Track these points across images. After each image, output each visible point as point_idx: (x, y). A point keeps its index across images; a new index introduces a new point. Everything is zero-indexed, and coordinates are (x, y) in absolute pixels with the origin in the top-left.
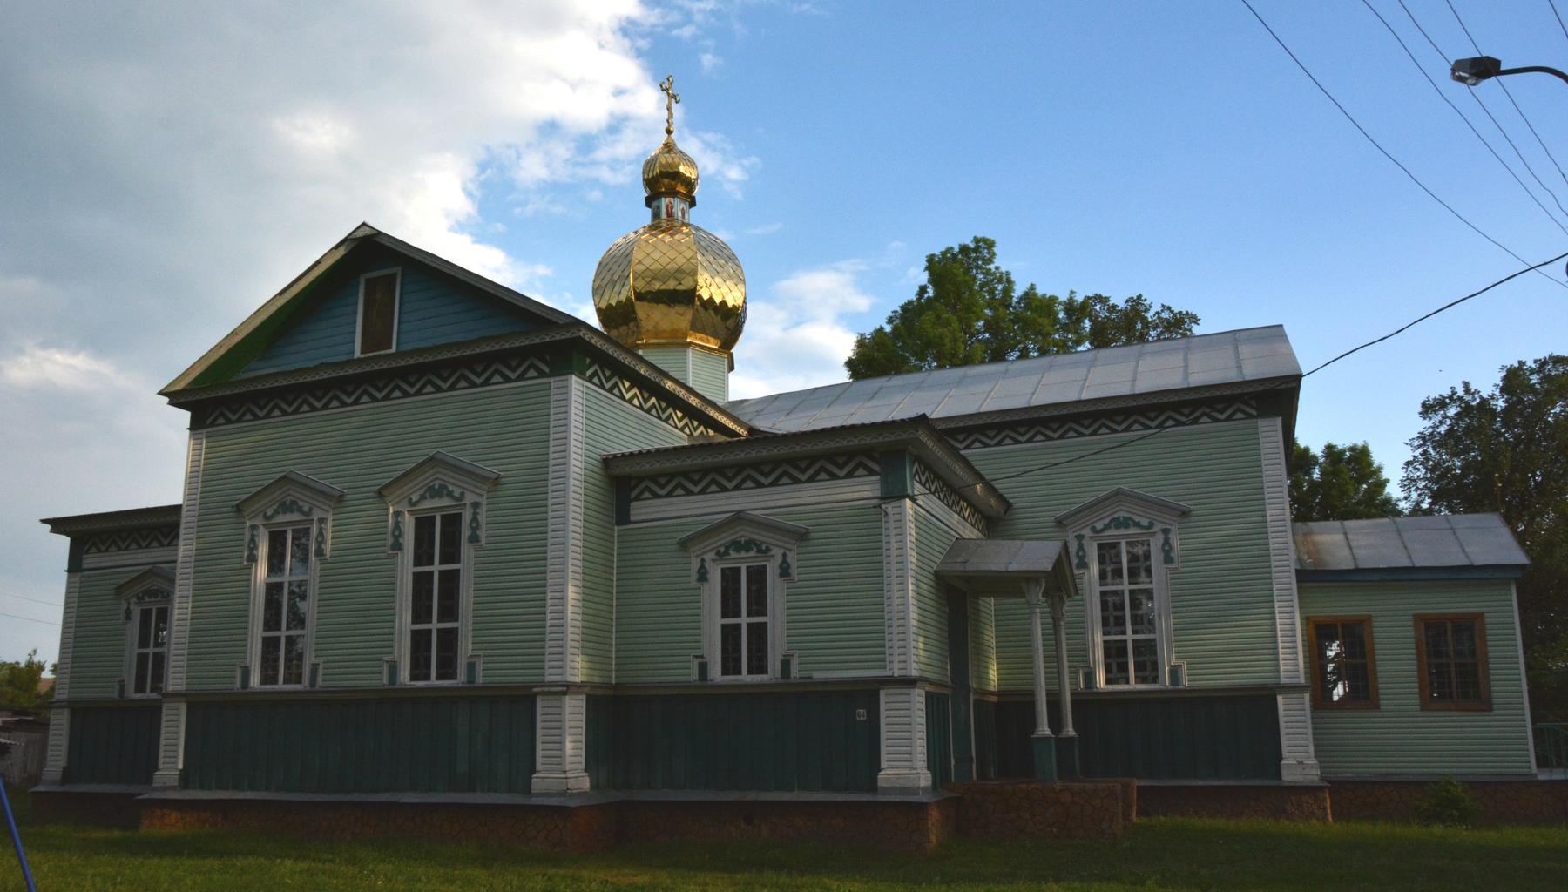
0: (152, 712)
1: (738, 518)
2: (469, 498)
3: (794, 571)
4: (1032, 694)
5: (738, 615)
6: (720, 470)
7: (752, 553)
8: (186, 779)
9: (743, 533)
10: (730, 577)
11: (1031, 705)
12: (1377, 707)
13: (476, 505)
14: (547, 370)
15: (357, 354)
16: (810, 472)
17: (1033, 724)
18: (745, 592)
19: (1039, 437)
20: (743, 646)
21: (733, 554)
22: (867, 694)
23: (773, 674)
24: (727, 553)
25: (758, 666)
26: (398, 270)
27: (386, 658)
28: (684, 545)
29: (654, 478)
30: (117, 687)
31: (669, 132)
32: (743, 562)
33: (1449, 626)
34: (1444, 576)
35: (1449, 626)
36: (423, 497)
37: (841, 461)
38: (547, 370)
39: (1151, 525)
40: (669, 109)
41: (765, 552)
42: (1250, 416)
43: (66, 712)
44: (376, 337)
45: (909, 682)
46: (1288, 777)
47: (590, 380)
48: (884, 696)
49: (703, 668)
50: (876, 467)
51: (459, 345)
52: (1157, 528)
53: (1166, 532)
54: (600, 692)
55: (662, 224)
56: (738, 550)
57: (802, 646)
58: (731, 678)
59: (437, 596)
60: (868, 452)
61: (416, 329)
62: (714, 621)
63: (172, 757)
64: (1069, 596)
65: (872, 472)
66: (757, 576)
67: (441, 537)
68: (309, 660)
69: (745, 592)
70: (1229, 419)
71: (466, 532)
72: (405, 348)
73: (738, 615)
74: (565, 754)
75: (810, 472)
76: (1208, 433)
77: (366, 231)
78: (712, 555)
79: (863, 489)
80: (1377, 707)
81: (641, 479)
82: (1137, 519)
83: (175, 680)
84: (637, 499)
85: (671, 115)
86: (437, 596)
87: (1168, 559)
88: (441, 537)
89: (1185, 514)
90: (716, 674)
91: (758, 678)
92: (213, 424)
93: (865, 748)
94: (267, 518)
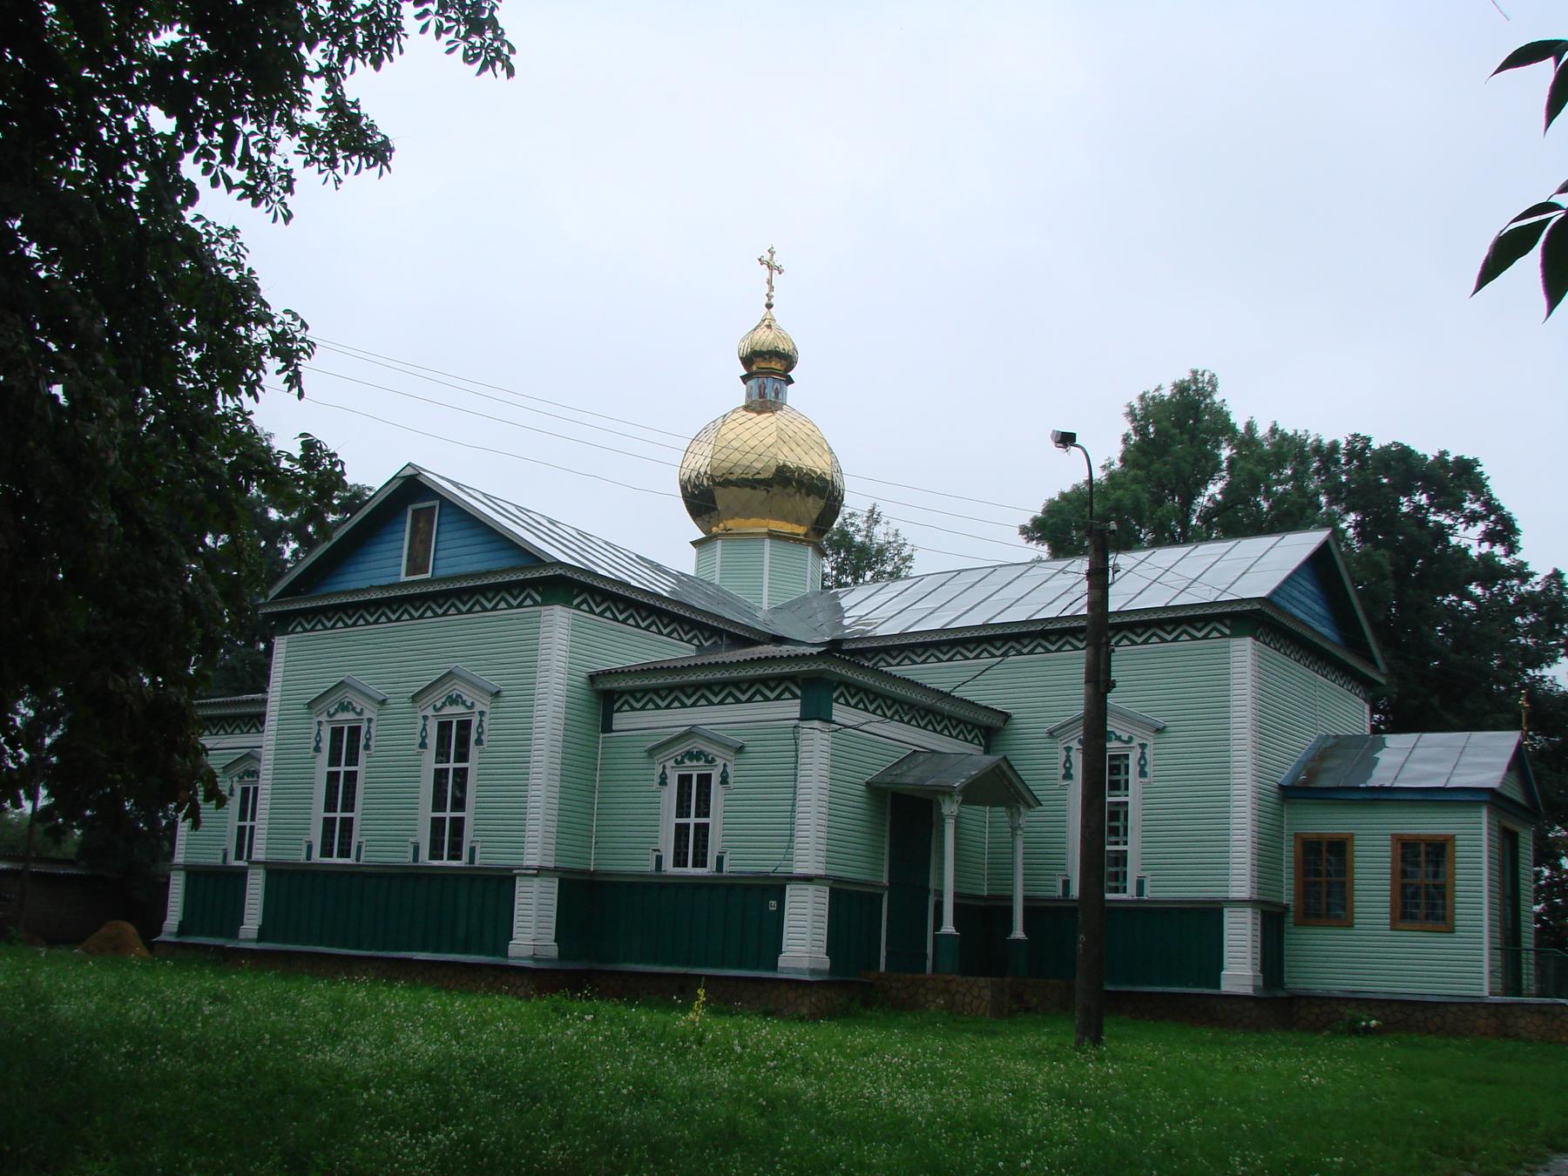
0: (240, 876)
1: (691, 732)
2: (478, 707)
3: (731, 780)
4: (1010, 898)
5: (688, 816)
6: (682, 688)
7: (702, 763)
8: (262, 935)
9: (698, 745)
10: (684, 781)
11: (1009, 911)
12: (1351, 925)
13: (482, 713)
14: (539, 599)
15: (403, 578)
16: (721, 697)
17: (1009, 928)
18: (694, 795)
19: (1068, 647)
20: (693, 842)
21: (687, 763)
22: (773, 888)
23: (709, 870)
24: (682, 762)
25: (700, 861)
26: (437, 503)
27: (412, 839)
28: (652, 752)
29: (632, 692)
30: (411, 850)
31: (769, 306)
32: (695, 769)
33: (1423, 848)
34: (1468, 797)
35: (1423, 848)
36: (444, 704)
37: (772, 684)
38: (539, 599)
39: (1130, 739)
40: (770, 282)
41: (711, 762)
42: (1224, 635)
43: (183, 873)
44: (416, 565)
45: (807, 879)
46: (1227, 986)
47: (578, 607)
48: (790, 890)
49: (659, 860)
50: (799, 693)
51: (488, 573)
52: (1135, 743)
53: (1143, 746)
54: (570, 876)
55: (763, 403)
56: (691, 759)
57: (735, 848)
58: (436, 863)
59: (450, 790)
60: (792, 678)
61: (454, 558)
62: (670, 821)
63: (252, 921)
64: (1029, 806)
65: (795, 696)
66: (705, 780)
67: (456, 739)
68: (356, 838)
69: (694, 795)
70: (1205, 637)
71: (473, 736)
72: (439, 573)
73: (688, 816)
74: (533, 926)
75: (721, 697)
76: (1185, 650)
77: (410, 471)
78: (672, 763)
79: (791, 708)
80: (1351, 925)
81: (622, 693)
82: (1118, 733)
83: (259, 854)
84: (619, 710)
85: (772, 288)
86: (450, 790)
87: (1143, 774)
88: (456, 739)
89: (1160, 730)
90: (669, 867)
91: (699, 871)
92: (293, 632)
93: (768, 935)
94: (330, 715)
